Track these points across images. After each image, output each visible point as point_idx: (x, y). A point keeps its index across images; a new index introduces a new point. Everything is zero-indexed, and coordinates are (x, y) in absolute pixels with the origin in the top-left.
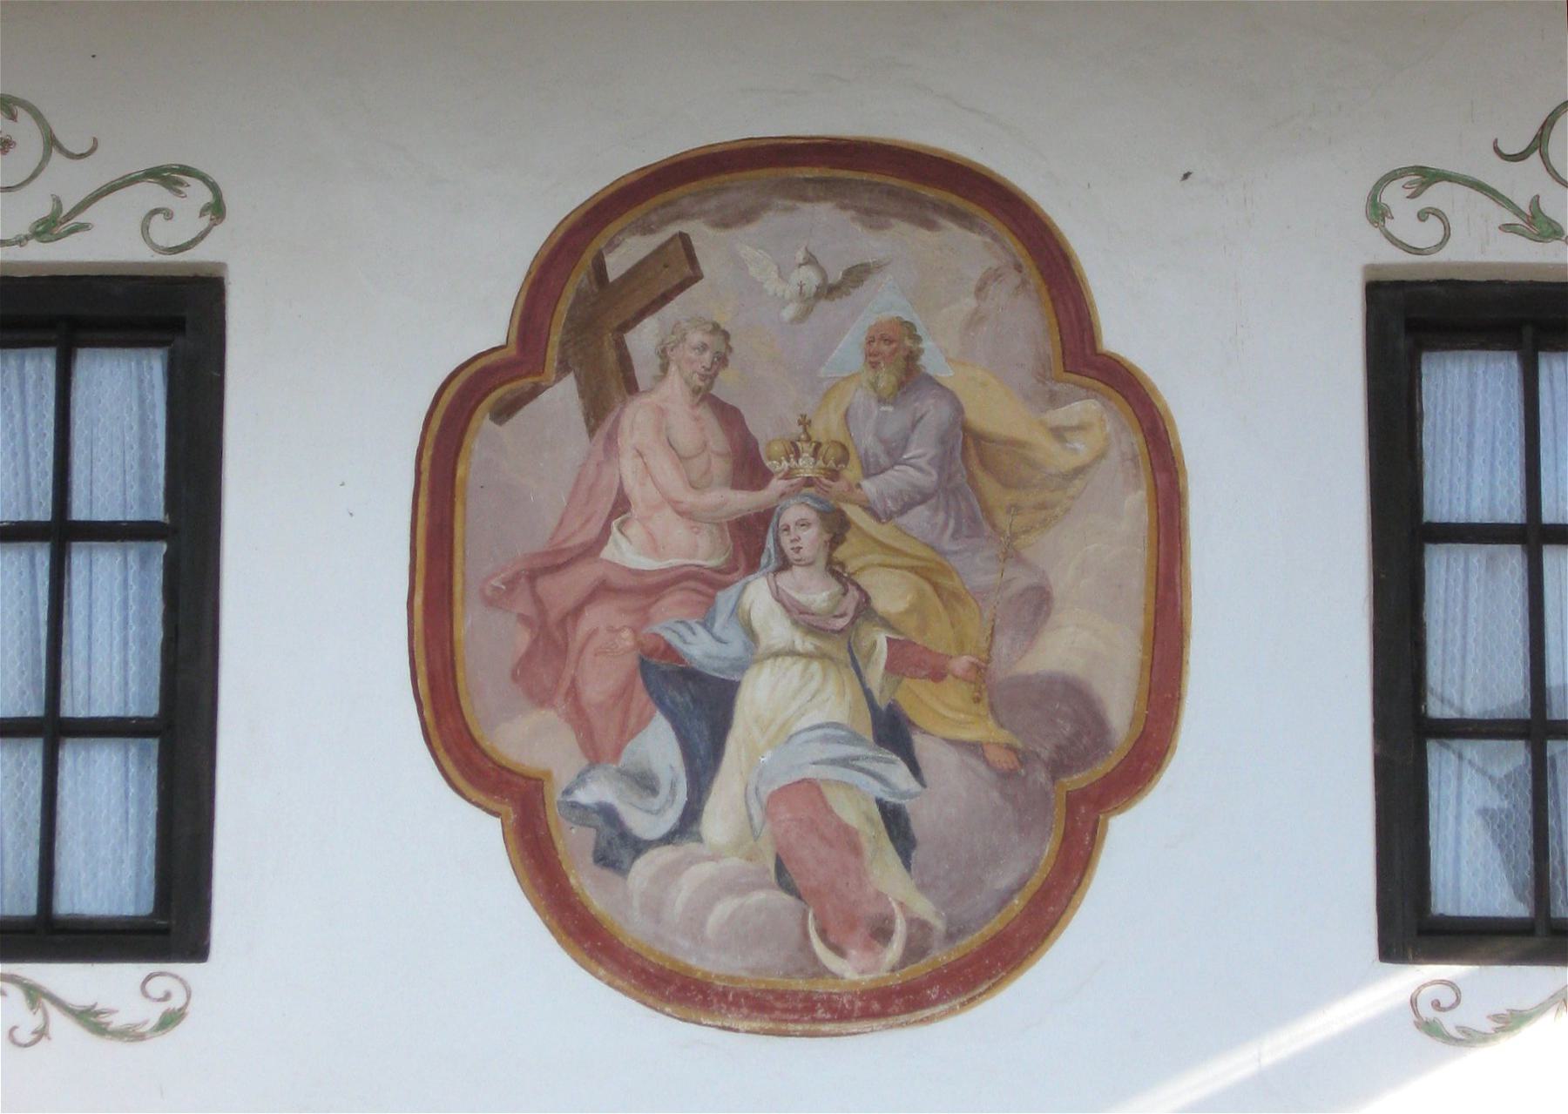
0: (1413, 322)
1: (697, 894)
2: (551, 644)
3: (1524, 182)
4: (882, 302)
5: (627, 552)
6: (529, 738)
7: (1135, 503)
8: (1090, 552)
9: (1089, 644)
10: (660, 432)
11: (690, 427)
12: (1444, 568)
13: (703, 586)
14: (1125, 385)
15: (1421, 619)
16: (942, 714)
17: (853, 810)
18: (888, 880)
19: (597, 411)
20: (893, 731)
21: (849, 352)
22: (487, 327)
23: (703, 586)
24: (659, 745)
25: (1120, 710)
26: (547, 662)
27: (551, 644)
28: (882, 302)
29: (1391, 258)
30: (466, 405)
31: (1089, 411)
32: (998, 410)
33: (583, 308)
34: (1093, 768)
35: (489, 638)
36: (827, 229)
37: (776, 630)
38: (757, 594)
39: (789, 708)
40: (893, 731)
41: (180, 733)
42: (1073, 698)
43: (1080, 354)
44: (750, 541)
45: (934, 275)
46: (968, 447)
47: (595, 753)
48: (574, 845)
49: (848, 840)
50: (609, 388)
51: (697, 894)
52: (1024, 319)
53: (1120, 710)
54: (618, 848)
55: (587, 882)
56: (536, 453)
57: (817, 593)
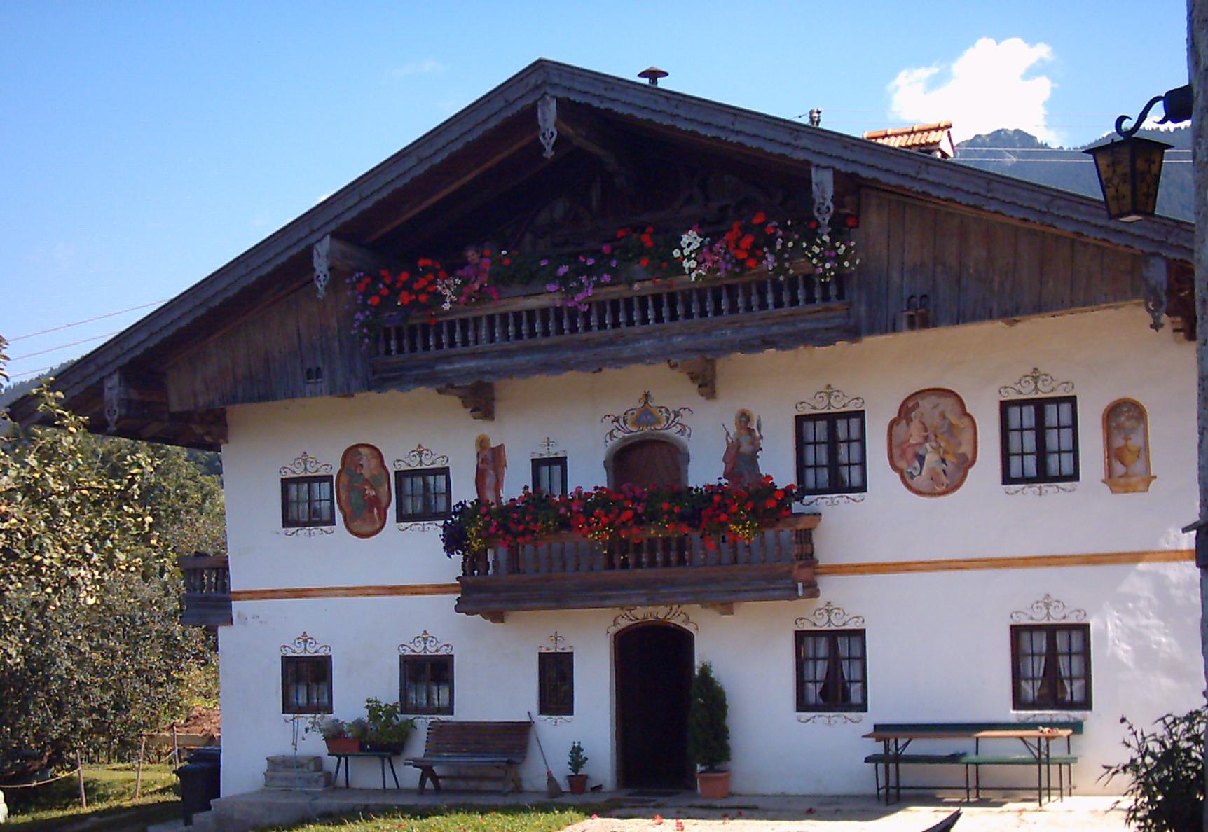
0: (1005, 406)
1: (921, 481)
2: (903, 453)
3: (1018, 387)
4: (941, 408)
5: (911, 441)
6: (902, 464)
7: (971, 431)
8: (966, 437)
9: (966, 448)
10: (915, 425)
11: (920, 426)
12: (859, 677)
13: (921, 444)
14: (969, 416)
15: (79, 361)
16: (949, 458)
17: (315, 745)
18: (944, 478)
19: (908, 424)
20: (943, 461)
21: (937, 412)
22: (895, 415)
23: (921, 444)
24: (917, 464)
25: (970, 457)
26: (903, 454)
27: (903, 453)
28: (941, 408)
29: (1013, 623)
30: (893, 424)
31: (966, 421)
32: (954, 420)
33: (906, 411)
34: (966, 463)
35: (896, 452)
36: (933, 399)
37: (930, 449)
38: (927, 445)
39: (931, 459)
40: (943, 461)
41: (862, 464)
42: (964, 455)
43: (965, 414)
44: (926, 439)
45: (947, 404)
46: (951, 425)
47: (909, 465)
48: (907, 476)
49: (938, 475)
50: (909, 421)
51: (921, 481)
52: (957, 409)
53: (970, 457)
54: (912, 477)
55: (909, 481)
56: (901, 429)
57: (934, 445)
